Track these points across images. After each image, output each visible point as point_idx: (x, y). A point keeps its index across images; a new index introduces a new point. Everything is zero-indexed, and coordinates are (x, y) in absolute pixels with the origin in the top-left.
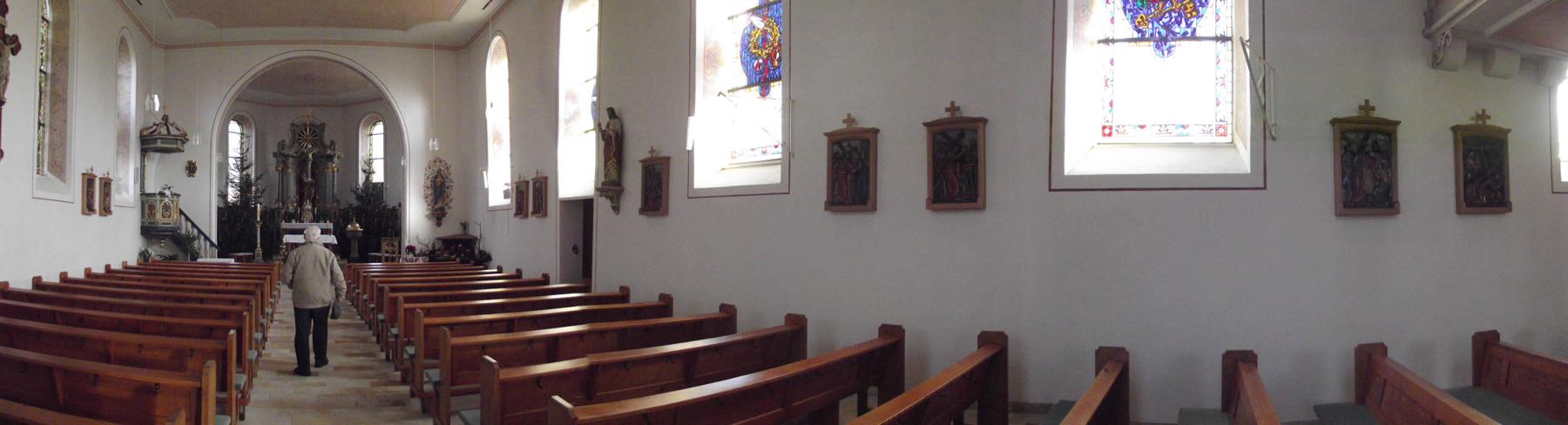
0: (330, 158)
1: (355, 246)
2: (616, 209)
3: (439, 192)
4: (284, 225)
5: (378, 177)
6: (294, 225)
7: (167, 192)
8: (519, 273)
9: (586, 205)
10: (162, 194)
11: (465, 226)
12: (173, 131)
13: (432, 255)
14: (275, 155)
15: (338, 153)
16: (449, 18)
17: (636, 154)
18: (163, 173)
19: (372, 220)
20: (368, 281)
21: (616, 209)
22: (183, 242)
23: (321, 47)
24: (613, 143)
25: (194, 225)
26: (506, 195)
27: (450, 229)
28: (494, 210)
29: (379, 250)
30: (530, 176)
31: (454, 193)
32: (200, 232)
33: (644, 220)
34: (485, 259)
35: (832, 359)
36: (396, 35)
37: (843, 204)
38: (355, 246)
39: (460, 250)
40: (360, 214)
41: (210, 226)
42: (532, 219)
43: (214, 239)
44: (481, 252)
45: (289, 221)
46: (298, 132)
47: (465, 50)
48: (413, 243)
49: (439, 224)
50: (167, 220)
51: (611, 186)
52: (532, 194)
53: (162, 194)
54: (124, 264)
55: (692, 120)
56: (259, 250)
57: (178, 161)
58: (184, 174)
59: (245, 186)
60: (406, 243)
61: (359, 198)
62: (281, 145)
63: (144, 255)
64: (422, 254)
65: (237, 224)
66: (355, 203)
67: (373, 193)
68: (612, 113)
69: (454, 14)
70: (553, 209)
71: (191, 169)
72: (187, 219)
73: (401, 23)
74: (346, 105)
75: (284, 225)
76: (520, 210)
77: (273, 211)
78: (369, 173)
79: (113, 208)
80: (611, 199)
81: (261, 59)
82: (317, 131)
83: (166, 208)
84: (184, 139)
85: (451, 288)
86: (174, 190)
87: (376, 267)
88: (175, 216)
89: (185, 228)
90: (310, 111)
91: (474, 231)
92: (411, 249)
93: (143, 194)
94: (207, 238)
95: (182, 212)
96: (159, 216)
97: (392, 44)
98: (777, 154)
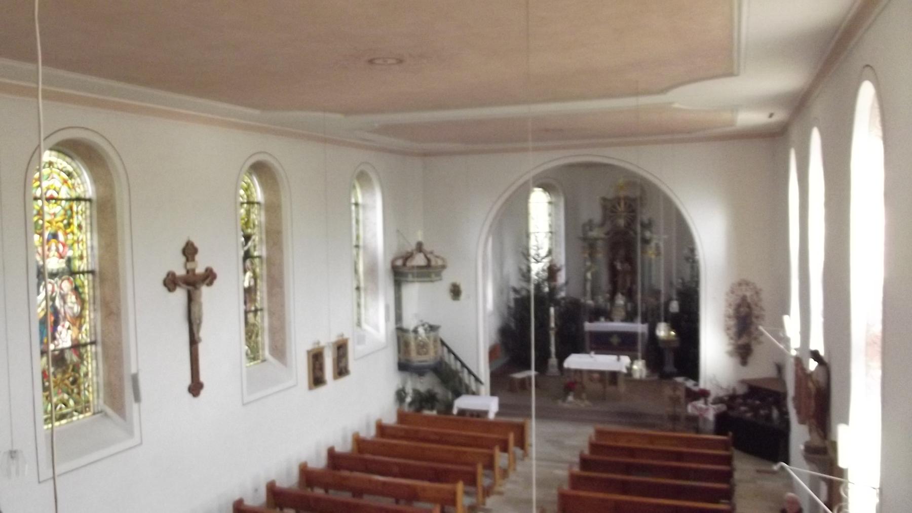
22: (450, 377)
46: (610, 208)
57: (442, 288)
58: (447, 296)
71: (456, 292)
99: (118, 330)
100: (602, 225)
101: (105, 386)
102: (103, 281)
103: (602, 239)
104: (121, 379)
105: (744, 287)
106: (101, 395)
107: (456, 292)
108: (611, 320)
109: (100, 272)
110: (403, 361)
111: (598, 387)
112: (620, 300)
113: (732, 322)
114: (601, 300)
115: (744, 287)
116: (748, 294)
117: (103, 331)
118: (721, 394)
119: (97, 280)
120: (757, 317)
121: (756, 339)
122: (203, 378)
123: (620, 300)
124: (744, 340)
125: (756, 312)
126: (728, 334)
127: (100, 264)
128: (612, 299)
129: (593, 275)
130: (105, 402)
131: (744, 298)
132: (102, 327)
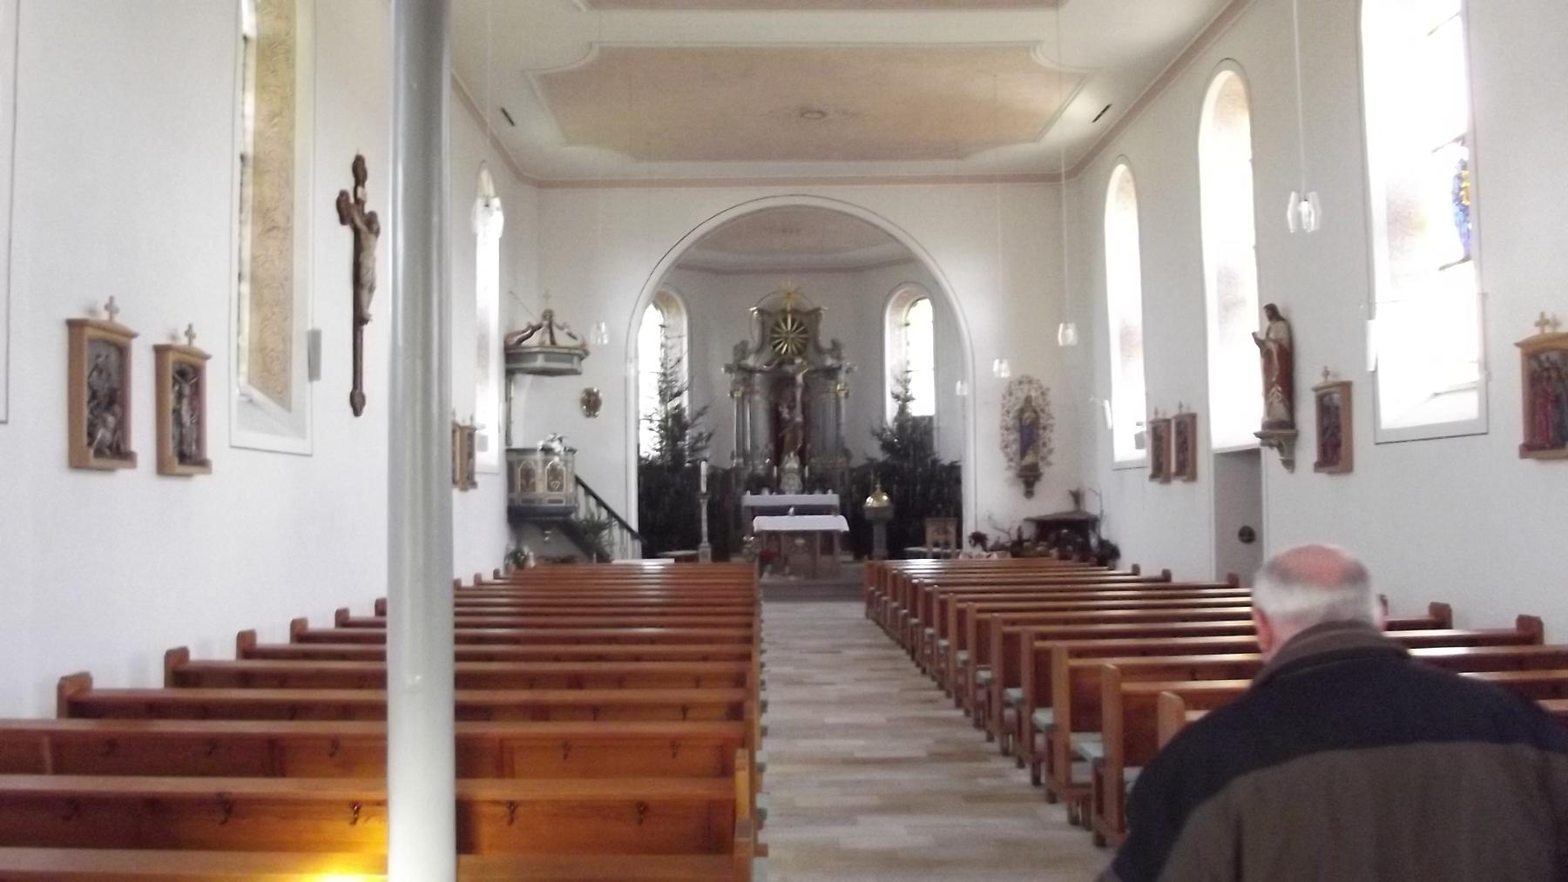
0: (831, 373)
1: (879, 534)
2: (1289, 464)
3: (1028, 434)
4: (749, 499)
5: (923, 406)
6: (766, 498)
7: (557, 446)
8: (1166, 576)
9: (1250, 456)
10: (547, 450)
11: (1077, 497)
12: (562, 339)
13: (1017, 548)
14: (729, 369)
15: (847, 363)
16: (1036, 138)
17: (1308, 379)
18: (546, 413)
19: (915, 484)
20: (912, 591)
21: (1289, 464)
22: (584, 537)
23: (815, 190)
24: (1280, 363)
25: (600, 503)
26: (1139, 443)
27: (1050, 502)
28: (1122, 468)
29: (922, 543)
30: (1172, 412)
31: (1056, 438)
32: (611, 513)
33: (1323, 478)
34: (1108, 554)
35: (1213, 564)
36: (948, 166)
37: (1542, 448)
38: (879, 534)
39: (1072, 537)
40: (888, 475)
41: (629, 508)
42: (1177, 485)
43: (634, 525)
44: (1103, 544)
45: (756, 492)
46: (771, 321)
47: (1072, 176)
48: (983, 530)
49: (1029, 493)
50: (555, 495)
51: (1280, 432)
52: (1174, 444)
53: (547, 450)
54: (477, 578)
55: (1374, 327)
56: (705, 546)
57: (568, 390)
58: (577, 411)
59: (673, 427)
60: (969, 528)
61: (887, 446)
62: (741, 350)
63: (516, 558)
64: (998, 547)
65: (674, 501)
66: (880, 456)
67: (912, 440)
68: (1272, 312)
69: (1042, 134)
70: (1205, 466)
71: (591, 403)
72: (589, 492)
73: (955, 151)
74: (856, 269)
75: (749, 499)
76: (1159, 471)
77: (727, 473)
78: (903, 399)
79: (478, 478)
80: (1280, 447)
81: (710, 207)
82: (807, 321)
83: (554, 473)
84: (582, 353)
85: (1067, 622)
86: (568, 443)
87: (921, 567)
88: (570, 487)
89: (585, 509)
90: (789, 283)
91: (1092, 507)
92: (979, 539)
93: (509, 451)
94: (624, 525)
95: (578, 481)
96: (541, 488)
97: (938, 179)
98: (1474, 375)
99: (286, 253)
100: (759, 351)
101: (251, 352)
102: (259, 173)
103: (761, 371)
104: (287, 339)
105: (1026, 387)
106: (244, 368)
107: (591, 403)
108: (780, 492)
109: (256, 158)
110: (519, 503)
111: (802, 559)
112: (792, 463)
113: (1014, 436)
114: (761, 466)
115: (1026, 387)
116: (1033, 394)
117: (254, 258)
118: (1004, 539)
119: (249, 170)
120: (1045, 428)
121: (1043, 458)
122: (366, 390)
123: (792, 463)
124: (1029, 459)
125: (1042, 422)
126: (1007, 454)
127: (255, 145)
128: (778, 459)
129: (805, 377)
130: (250, 381)
131: (1028, 400)
132: (253, 246)
